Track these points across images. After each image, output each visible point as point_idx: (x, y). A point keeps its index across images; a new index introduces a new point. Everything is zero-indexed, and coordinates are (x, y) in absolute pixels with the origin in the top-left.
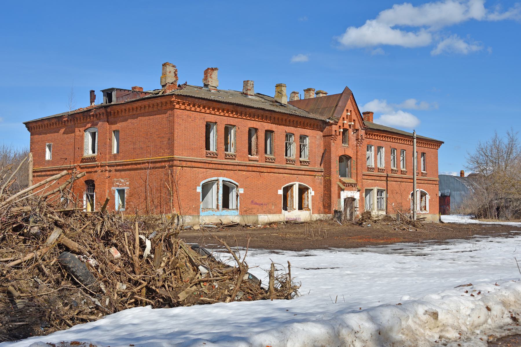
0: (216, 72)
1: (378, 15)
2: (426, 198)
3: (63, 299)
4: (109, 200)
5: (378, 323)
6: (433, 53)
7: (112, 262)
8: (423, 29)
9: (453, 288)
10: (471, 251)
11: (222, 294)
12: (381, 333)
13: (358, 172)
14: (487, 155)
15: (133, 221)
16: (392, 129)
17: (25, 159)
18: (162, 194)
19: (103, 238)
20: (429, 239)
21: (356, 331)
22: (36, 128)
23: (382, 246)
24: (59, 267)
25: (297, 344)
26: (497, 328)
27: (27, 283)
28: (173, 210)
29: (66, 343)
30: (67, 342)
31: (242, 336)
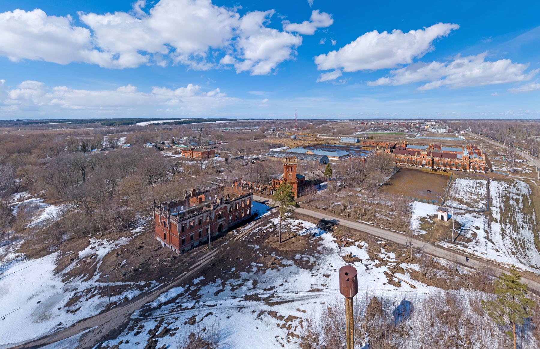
0: (308, 290)
1: (52, 15)
2: (323, 173)
3: (380, 159)
4: (194, 189)
5: (419, 62)
6: (213, 220)
7: (374, 196)
8: (253, 68)
9: (402, 66)
10: (388, 290)
11: (468, 327)
12: (429, 192)
13: (442, 256)
14: (288, 238)
15: (282, 323)
16: (36, 120)
17: (97, 346)
18: (512, 194)
19: (133, 245)
20: (262, 122)
21: (487, 245)
22: (74, 292)
23: (365, 222)
24: (519, 198)
25: (61, 348)
26: (199, 59)
27: (239, 185)
28: (262, 313)
29: (155, 54)
30: (157, 52)
31: (210, 308)
